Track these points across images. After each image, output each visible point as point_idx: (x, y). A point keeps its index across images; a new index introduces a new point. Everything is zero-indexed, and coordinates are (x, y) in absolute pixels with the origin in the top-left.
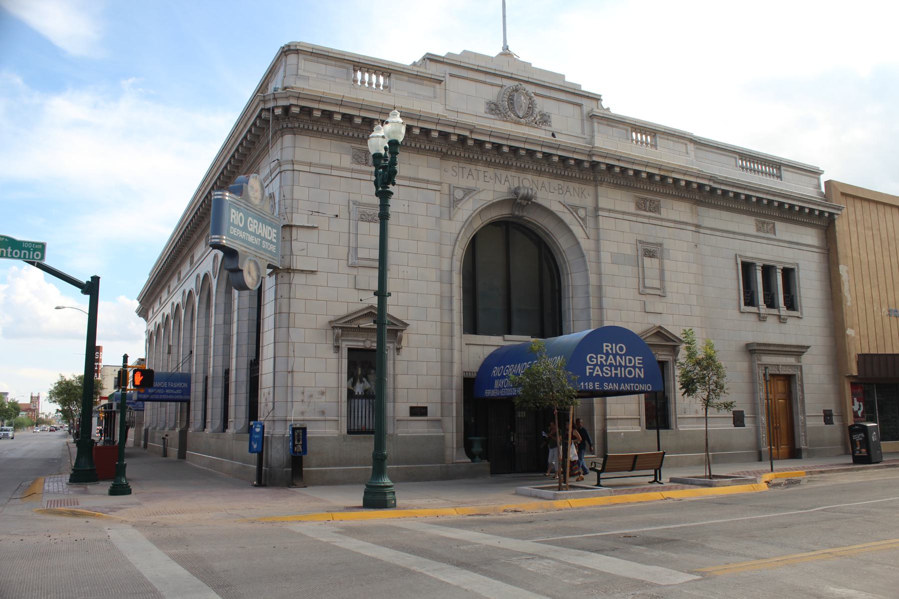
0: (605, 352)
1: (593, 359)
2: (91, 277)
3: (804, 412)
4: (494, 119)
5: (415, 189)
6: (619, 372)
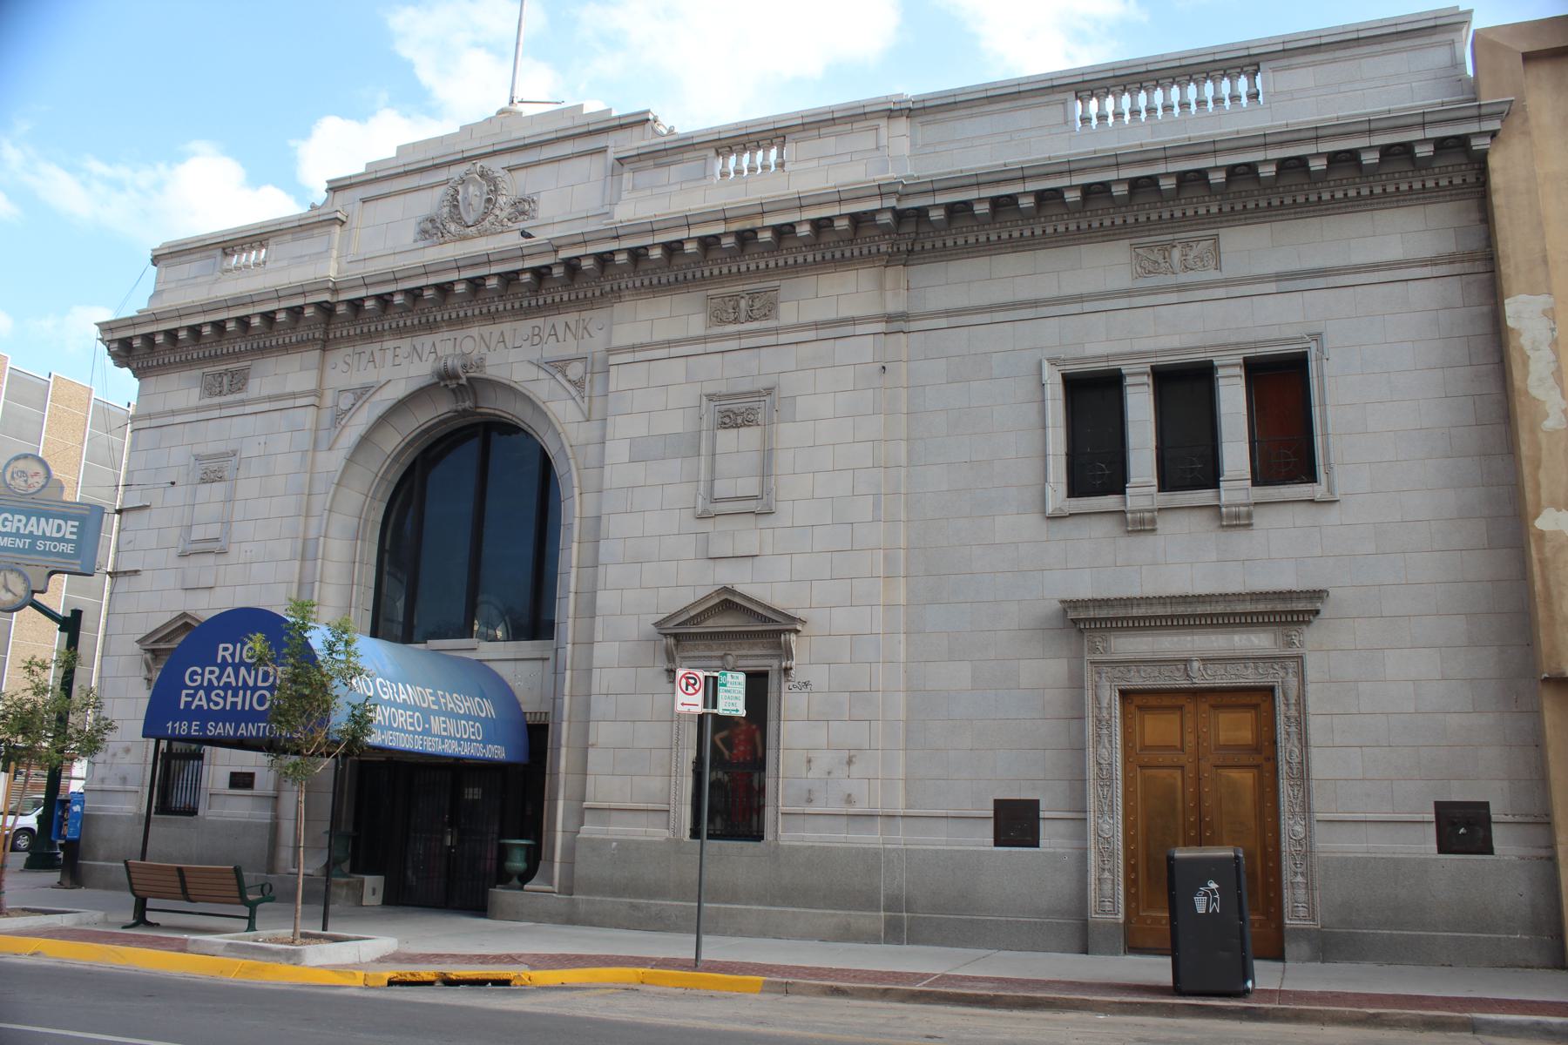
0: (219, 661)
1: (195, 677)
2: (72, 611)
3: (1307, 809)
4: (424, 248)
5: (278, 412)
6: (239, 700)
